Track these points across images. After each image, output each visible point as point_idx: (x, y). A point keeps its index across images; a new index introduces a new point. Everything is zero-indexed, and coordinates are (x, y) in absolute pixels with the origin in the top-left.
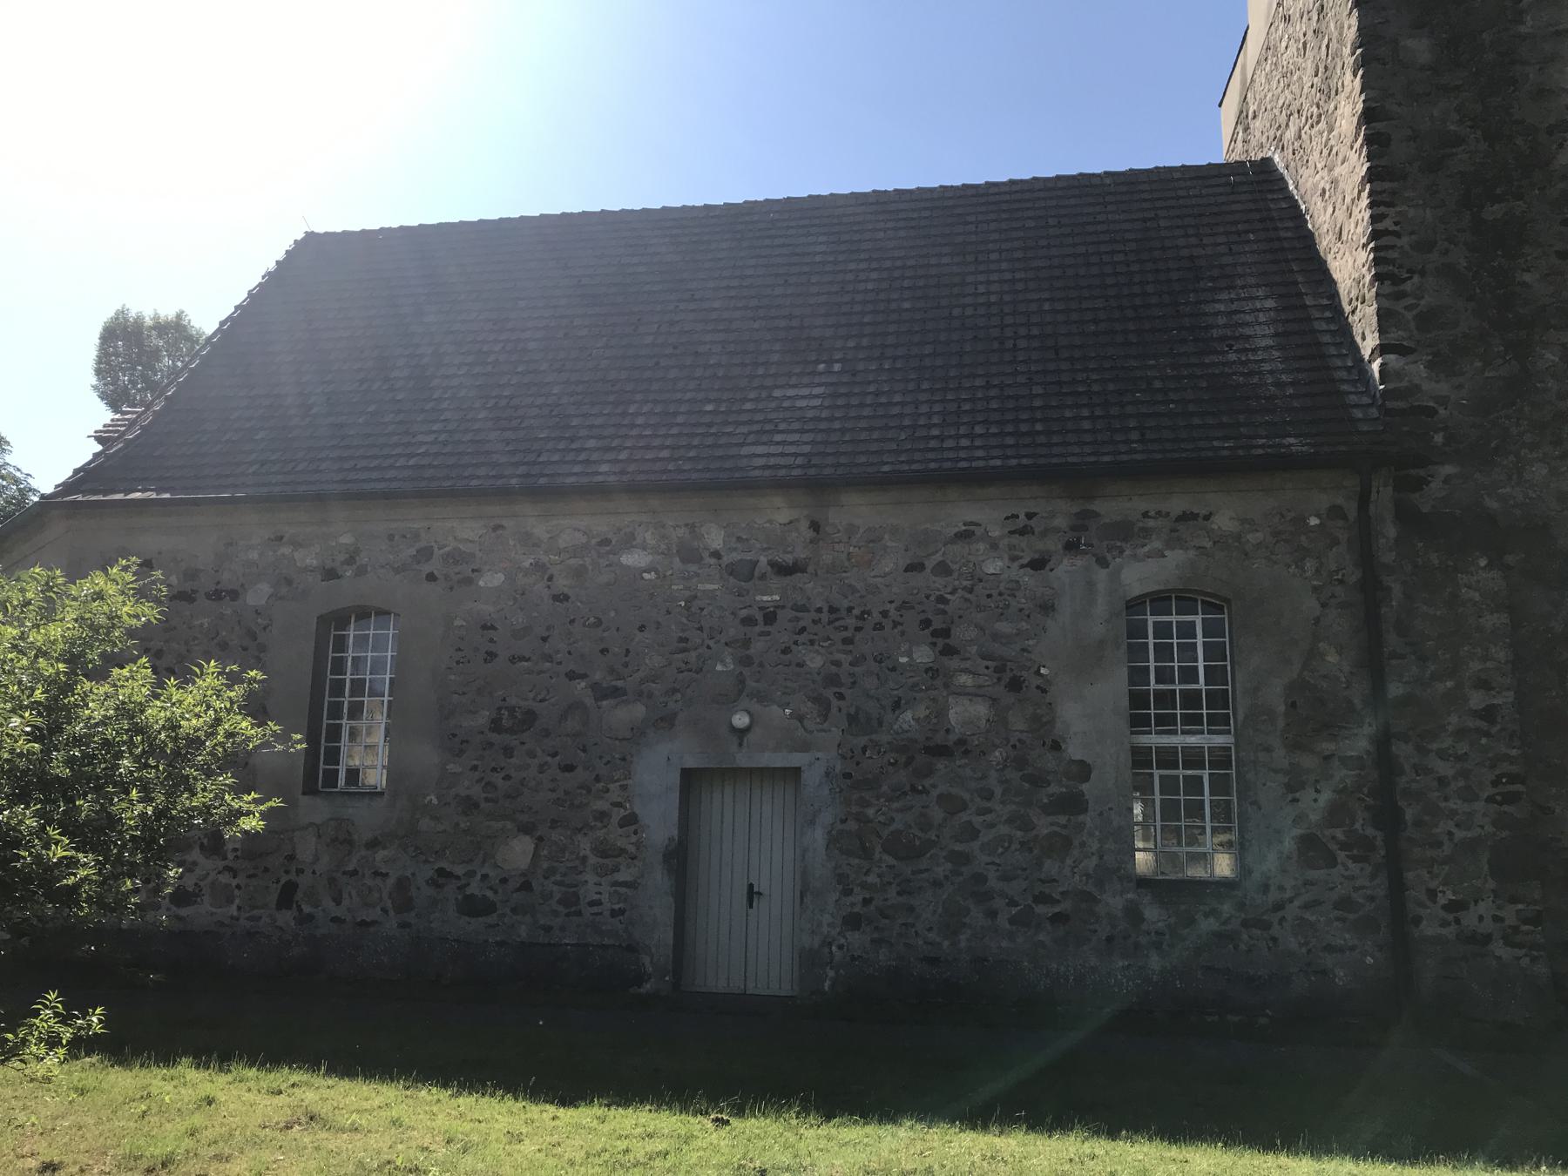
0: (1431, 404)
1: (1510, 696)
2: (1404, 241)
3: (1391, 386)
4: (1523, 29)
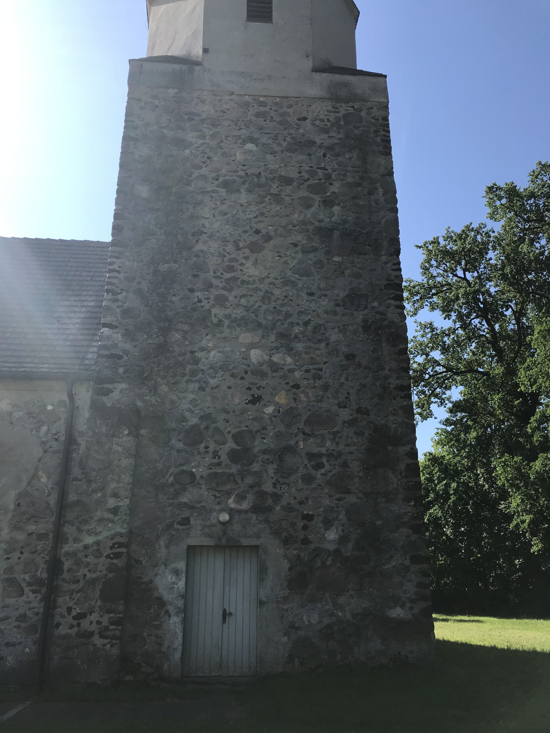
0: (121, 354)
1: (127, 501)
2: (121, 276)
3: (103, 343)
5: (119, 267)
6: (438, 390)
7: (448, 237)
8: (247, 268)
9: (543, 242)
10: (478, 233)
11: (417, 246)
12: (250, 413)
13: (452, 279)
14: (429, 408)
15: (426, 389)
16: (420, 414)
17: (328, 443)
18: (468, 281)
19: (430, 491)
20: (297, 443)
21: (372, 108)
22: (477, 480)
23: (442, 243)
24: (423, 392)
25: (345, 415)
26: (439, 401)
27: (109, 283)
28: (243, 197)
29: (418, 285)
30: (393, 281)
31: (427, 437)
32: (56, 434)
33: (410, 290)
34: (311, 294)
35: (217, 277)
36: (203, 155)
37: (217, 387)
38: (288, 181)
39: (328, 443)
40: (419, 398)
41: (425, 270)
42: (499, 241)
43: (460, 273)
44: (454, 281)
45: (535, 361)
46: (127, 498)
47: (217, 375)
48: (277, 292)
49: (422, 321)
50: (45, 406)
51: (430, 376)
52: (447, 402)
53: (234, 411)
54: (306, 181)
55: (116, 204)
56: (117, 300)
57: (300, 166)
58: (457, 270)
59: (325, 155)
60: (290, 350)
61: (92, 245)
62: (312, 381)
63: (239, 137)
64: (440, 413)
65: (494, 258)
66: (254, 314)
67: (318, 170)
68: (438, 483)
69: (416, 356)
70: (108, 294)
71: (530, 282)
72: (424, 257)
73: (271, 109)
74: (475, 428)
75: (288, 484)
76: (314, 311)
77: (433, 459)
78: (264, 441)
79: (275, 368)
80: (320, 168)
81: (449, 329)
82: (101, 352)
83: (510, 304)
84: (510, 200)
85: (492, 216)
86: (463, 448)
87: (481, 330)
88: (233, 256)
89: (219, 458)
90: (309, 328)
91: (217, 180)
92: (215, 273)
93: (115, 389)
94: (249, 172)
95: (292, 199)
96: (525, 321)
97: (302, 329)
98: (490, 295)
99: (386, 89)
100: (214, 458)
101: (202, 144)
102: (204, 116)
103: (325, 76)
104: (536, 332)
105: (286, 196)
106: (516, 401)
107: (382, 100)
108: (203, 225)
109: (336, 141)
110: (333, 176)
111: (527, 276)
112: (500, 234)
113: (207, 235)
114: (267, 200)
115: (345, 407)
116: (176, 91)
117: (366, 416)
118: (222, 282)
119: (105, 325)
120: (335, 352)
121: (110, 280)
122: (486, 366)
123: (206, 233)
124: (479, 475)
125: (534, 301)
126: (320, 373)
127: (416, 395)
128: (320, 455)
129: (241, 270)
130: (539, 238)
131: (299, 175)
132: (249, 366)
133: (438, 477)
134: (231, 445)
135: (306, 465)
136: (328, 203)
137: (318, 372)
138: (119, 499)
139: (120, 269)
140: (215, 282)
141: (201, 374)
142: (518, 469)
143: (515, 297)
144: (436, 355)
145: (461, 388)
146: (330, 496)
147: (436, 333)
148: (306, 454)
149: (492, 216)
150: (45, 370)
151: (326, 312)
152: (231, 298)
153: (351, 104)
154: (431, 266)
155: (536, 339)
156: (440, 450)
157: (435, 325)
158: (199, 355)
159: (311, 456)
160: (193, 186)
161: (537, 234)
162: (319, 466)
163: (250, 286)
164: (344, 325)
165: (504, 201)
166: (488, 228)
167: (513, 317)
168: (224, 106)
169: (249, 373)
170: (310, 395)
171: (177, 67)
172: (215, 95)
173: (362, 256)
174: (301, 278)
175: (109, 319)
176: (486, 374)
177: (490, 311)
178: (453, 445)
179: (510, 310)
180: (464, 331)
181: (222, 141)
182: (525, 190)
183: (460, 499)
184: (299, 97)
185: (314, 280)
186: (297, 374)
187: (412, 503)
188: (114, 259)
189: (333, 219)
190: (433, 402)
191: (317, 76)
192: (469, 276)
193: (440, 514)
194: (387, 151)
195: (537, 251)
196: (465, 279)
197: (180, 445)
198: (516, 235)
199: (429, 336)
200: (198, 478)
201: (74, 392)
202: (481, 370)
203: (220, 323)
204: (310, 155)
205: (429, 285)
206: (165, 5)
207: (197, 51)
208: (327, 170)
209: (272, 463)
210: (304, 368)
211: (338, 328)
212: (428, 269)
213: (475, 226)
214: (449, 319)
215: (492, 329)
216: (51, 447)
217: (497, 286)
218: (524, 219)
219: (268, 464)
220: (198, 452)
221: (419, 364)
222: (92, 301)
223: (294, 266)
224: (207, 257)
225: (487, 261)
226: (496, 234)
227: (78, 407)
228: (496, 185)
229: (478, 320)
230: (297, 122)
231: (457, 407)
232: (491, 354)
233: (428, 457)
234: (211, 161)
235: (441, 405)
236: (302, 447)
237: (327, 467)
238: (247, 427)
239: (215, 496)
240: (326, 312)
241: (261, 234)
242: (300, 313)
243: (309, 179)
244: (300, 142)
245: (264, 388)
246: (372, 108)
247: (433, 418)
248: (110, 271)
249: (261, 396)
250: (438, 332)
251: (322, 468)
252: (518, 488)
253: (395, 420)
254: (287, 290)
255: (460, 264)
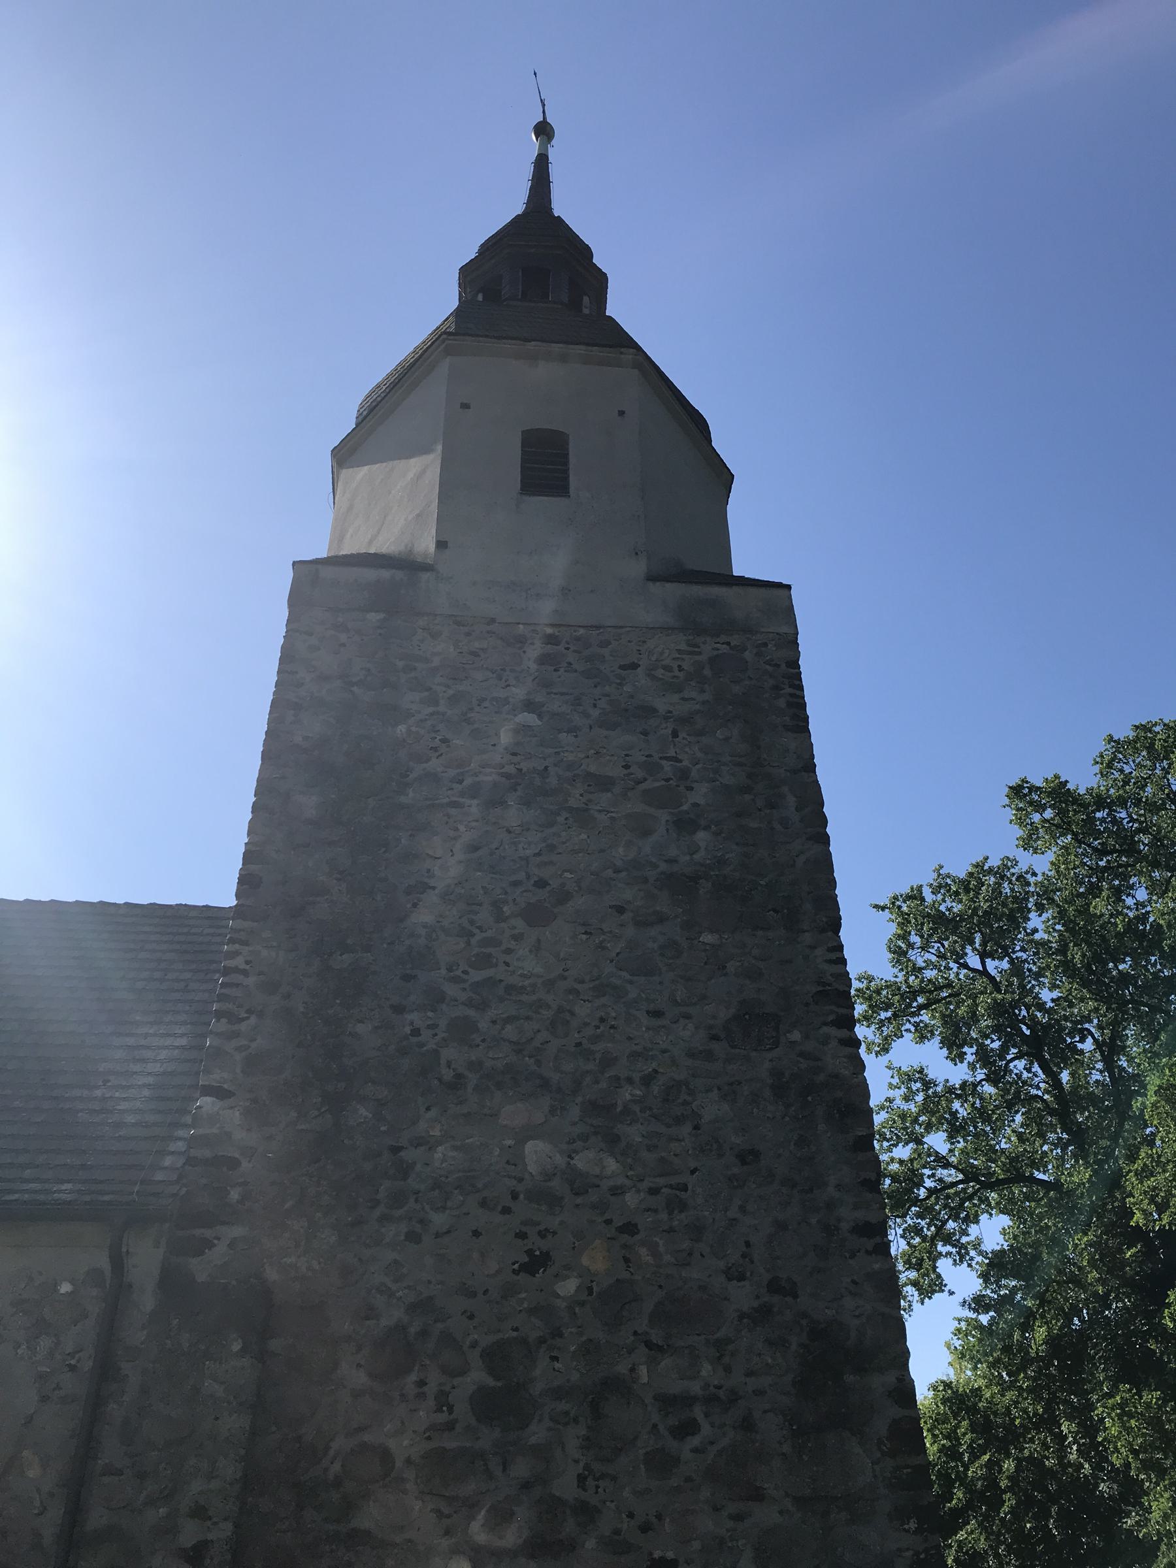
0: (237, 1156)
1: (227, 1528)
2: (251, 981)
3: (201, 1131)
4: (403, 799)
5: (247, 962)
6: (951, 1225)
7: (940, 886)
8: (518, 959)
9: (1142, 894)
10: (1002, 877)
11: (876, 907)
12: (523, 1295)
13: (958, 974)
14: (934, 1268)
15: (923, 1223)
16: (915, 1284)
17: (706, 1369)
18: (992, 979)
19: (954, 1481)
20: (632, 1370)
21: (765, 645)
22: (1062, 1451)
23: (927, 893)
24: (917, 1231)
25: (742, 1296)
26: (954, 1250)
27: (221, 998)
28: (513, 815)
29: (887, 987)
30: (829, 985)
31: (934, 1345)
32: (71, 1355)
33: (870, 998)
34: (657, 1014)
35: (455, 980)
36: (433, 735)
37: (448, 1232)
38: (603, 783)
39: (706, 1369)
40: (908, 1243)
41: (899, 955)
42: (1046, 894)
43: (974, 961)
44: (961, 976)
45: (1159, 1156)
46: (226, 1519)
47: (449, 1204)
48: (583, 1010)
49: (898, 1066)
50: (56, 1285)
51: (931, 1192)
52: (973, 1253)
53: (486, 1292)
54: (639, 782)
55: (248, 835)
56: (236, 1035)
57: (627, 755)
58: (966, 954)
59: (675, 734)
60: (612, 1141)
61: (193, 914)
62: (664, 1216)
63: (506, 701)
64: (962, 1280)
65: (1041, 927)
66: (532, 1060)
67: (664, 762)
68: (971, 1461)
69: (896, 1145)
70: (218, 1021)
71: (1124, 979)
72: (893, 929)
73: (567, 649)
74: (1043, 1316)
75: (614, 1479)
76: (664, 1051)
77: (956, 1399)
78: (557, 1365)
79: (580, 1184)
80: (666, 758)
81: (964, 1085)
82: (193, 1153)
83: (1087, 1026)
84: (1061, 813)
85: (1028, 843)
86: (1023, 1368)
87: (1031, 1086)
88: (489, 934)
89: (451, 1409)
90: (656, 1089)
91: (461, 782)
92: (450, 970)
93: (219, 1239)
94: (524, 766)
95: (612, 818)
96: (1125, 1065)
97: (638, 1092)
98: (1041, 1006)
99: (791, 608)
100: (439, 1410)
101: (432, 714)
102: (436, 661)
103: (674, 591)
104: (1152, 1089)
105: (600, 811)
106: (1129, 1249)
107: (784, 629)
108: (428, 871)
109: (697, 707)
110: (694, 774)
111: (1116, 967)
112: (1048, 878)
113: (436, 891)
114: (560, 819)
115: (741, 1278)
116: (382, 616)
117: (789, 1299)
118: (464, 989)
119: (207, 1091)
120: (715, 1146)
121: (223, 991)
122: (1050, 1167)
123: (434, 888)
124: (1066, 1437)
125: (1139, 1018)
126: (683, 1195)
127: (902, 1236)
128: (687, 1401)
129: (507, 964)
130: (1132, 887)
131: (626, 772)
132: (521, 1180)
133: (970, 1446)
134: (478, 1376)
135: (655, 1426)
136: (685, 825)
137: (678, 1193)
138: (209, 1523)
139: (247, 967)
140: (451, 990)
141: (412, 1200)
142: (1155, 1423)
143: (1096, 1010)
144: (937, 1141)
145: (1005, 1221)
146: (716, 1509)
147: (935, 1092)
148: (655, 1398)
149: (1028, 843)
150: (63, 1196)
151: (691, 1054)
152: (483, 1025)
153: (723, 638)
154: (911, 946)
155: (1154, 1105)
156: (969, 1373)
157: (931, 1075)
158: (409, 1155)
159: (667, 1402)
160: (411, 794)
161: (1125, 877)
162: (687, 1429)
163: (524, 998)
164: (731, 1084)
165: (1049, 814)
166: (1023, 866)
167: (1098, 1055)
168: (477, 645)
169: (522, 1196)
170: (661, 1249)
171: (385, 574)
172: (458, 623)
173: (760, 933)
174: (635, 978)
175: (216, 1077)
176: (1056, 1185)
177: (1047, 1044)
178: (998, 1361)
179: (1090, 1040)
180: (996, 1086)
181: (471, 709)
182: (1090, 791)
183: (1025, 1504)
184: (621, 627)
185: (660, 983)
186: (631, 1199)
187: (912, 1525)
188: (237, 946)
189: (696, 857)
190: (940, 1254)
191: (656, 588)
192: (991, 965)
193: (982, 1545)
194: (800, 723)
195: (1131, 915)
196: (984, 973)
197: (360, 1379)
198: (1081, 883)
199: (920, 1098)
200: (399, 1464)
201: (124, 1250)
202: (1041, 1176)
203: (457, 1084)
204: (645, 733)
205: (909, 987)
206: (366, 468)
207: (426, 544)
208: (681, 761)
209: (576, 1420)
210: (646, 1184)
211: (719, 1089)
212: (905, 953)
213: (994, 862)
214: (962, 1062)
215: (1056, 1083)
216: (58, 1387)
217: (1053, 987)
218: (1095, 849)
219: (566, 1424)
220: (402, 1395)
221: (901, 1162)
222: (182, 1035)
223: (618, 954)
224: (434, 936)
225: (1028, 934)
226: (1040, 878)
227: (130, 1286)
228: (1027, 782)
229: (1023, 1062)
230: (619, 671)
231: (997, 1266)
232: (1060, 1139)
233: (941, 1395)
234: (448, 746)
235: (961, 1261)
236: (645, 1380)
237: (706, 1429)
238: (516, 1329)
239: (439, 1514)
240: (691, 1054)
241: (548, 888)
242: (634, 1055)
243: (645, 780)
244: (626, 710)
245: (554, 1233)
246: (765, 645)
247: (946, 1293)
248: (226, 972)
249: (548, 1253)
250: (939, 1089)
251: (693, 1434)
252: (1162, 1473)
253: (858, 1307)
254: (604, 1006)
255: (972, 943)
